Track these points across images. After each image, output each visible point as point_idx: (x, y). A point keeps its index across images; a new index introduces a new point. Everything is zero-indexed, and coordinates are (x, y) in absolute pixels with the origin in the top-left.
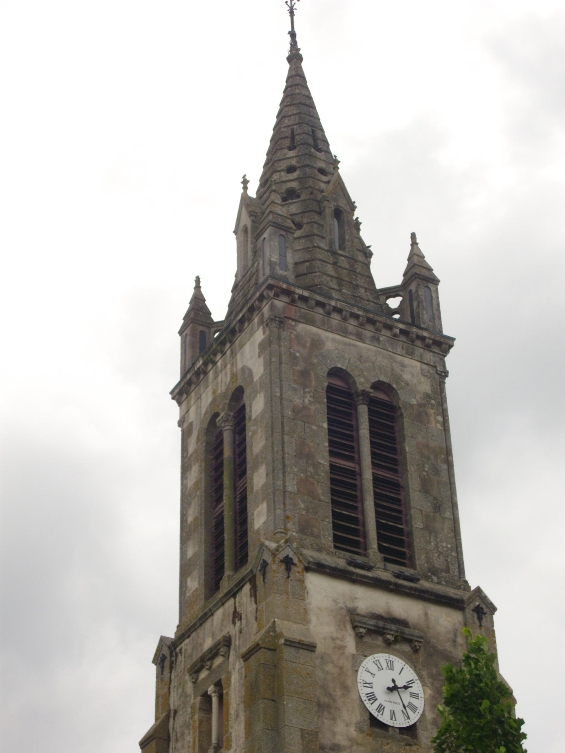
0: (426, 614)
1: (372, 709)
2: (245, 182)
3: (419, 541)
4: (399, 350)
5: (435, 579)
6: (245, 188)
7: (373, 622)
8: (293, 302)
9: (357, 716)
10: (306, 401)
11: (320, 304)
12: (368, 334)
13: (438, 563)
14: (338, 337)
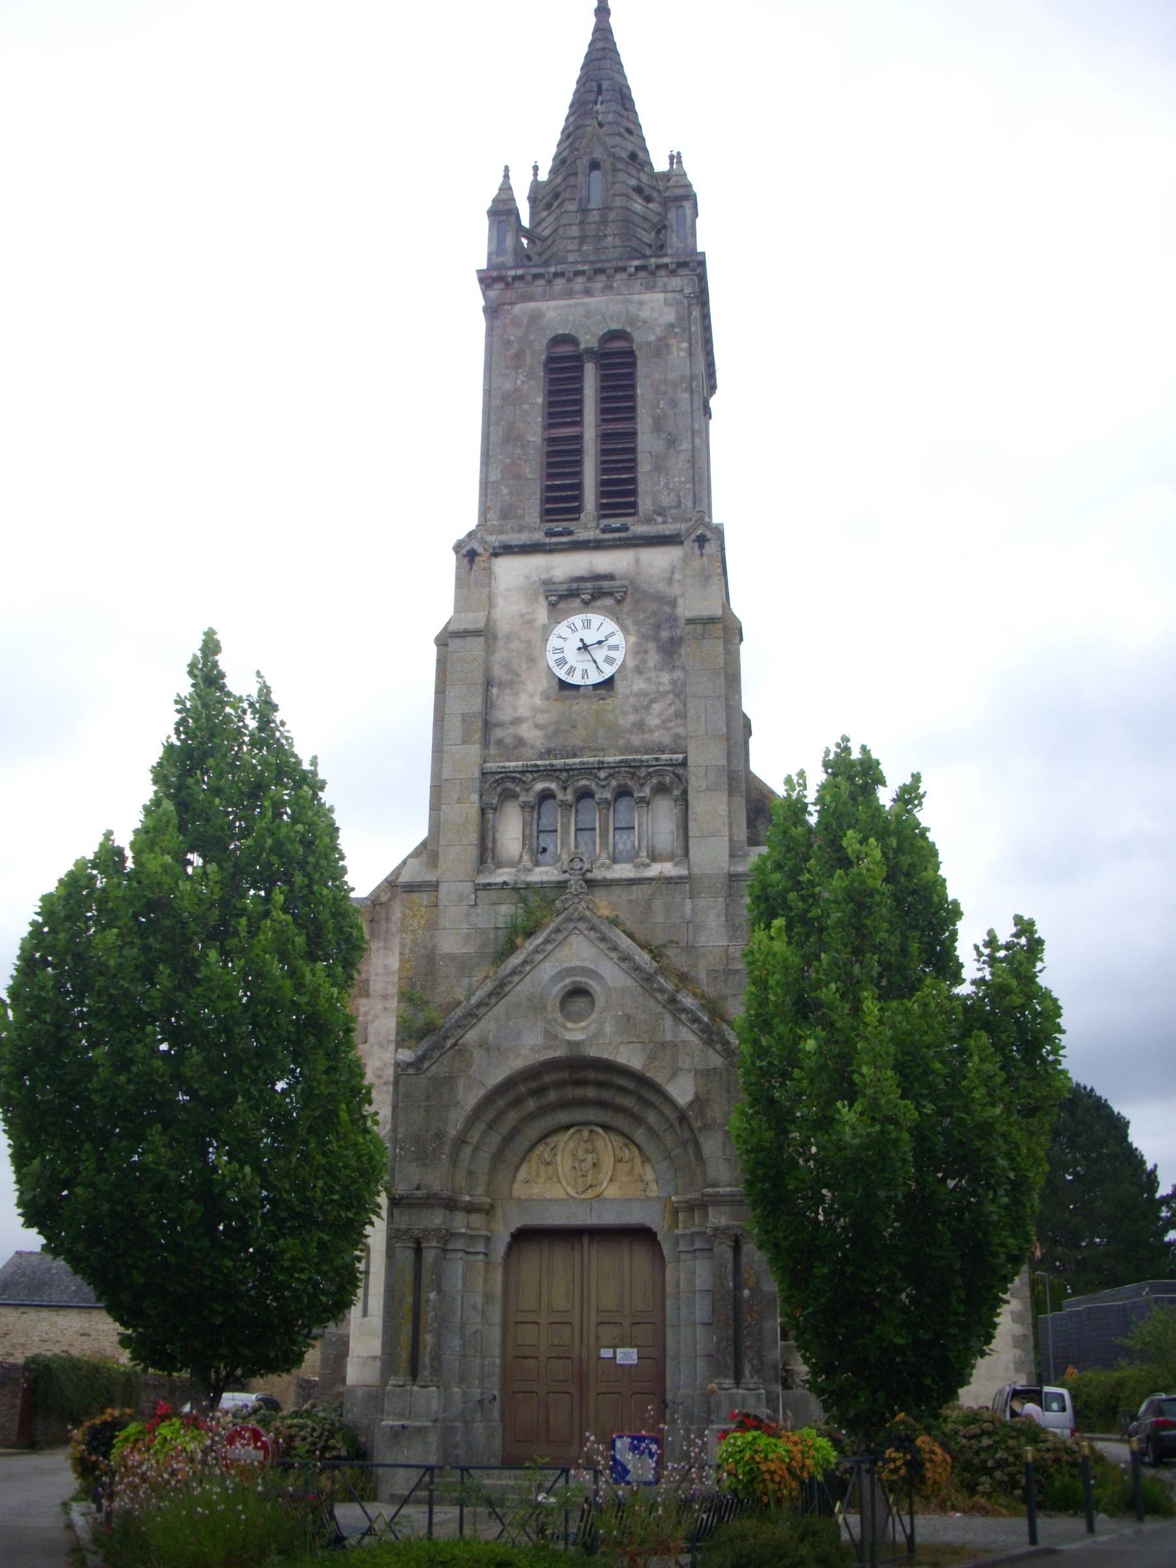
0: (637, 561)
1: (561, 674)
2: (536, 168)
3: (643, 486)
4: (637, 288)
5: (660, 519)
6: (535, 174)
7: (565, 586)
8: (507, 285)
9: (544, 684)
10: (519, 382)
11: (536, 277)
12: (598, 285)
13: (666, 500)
14: (561, 302)
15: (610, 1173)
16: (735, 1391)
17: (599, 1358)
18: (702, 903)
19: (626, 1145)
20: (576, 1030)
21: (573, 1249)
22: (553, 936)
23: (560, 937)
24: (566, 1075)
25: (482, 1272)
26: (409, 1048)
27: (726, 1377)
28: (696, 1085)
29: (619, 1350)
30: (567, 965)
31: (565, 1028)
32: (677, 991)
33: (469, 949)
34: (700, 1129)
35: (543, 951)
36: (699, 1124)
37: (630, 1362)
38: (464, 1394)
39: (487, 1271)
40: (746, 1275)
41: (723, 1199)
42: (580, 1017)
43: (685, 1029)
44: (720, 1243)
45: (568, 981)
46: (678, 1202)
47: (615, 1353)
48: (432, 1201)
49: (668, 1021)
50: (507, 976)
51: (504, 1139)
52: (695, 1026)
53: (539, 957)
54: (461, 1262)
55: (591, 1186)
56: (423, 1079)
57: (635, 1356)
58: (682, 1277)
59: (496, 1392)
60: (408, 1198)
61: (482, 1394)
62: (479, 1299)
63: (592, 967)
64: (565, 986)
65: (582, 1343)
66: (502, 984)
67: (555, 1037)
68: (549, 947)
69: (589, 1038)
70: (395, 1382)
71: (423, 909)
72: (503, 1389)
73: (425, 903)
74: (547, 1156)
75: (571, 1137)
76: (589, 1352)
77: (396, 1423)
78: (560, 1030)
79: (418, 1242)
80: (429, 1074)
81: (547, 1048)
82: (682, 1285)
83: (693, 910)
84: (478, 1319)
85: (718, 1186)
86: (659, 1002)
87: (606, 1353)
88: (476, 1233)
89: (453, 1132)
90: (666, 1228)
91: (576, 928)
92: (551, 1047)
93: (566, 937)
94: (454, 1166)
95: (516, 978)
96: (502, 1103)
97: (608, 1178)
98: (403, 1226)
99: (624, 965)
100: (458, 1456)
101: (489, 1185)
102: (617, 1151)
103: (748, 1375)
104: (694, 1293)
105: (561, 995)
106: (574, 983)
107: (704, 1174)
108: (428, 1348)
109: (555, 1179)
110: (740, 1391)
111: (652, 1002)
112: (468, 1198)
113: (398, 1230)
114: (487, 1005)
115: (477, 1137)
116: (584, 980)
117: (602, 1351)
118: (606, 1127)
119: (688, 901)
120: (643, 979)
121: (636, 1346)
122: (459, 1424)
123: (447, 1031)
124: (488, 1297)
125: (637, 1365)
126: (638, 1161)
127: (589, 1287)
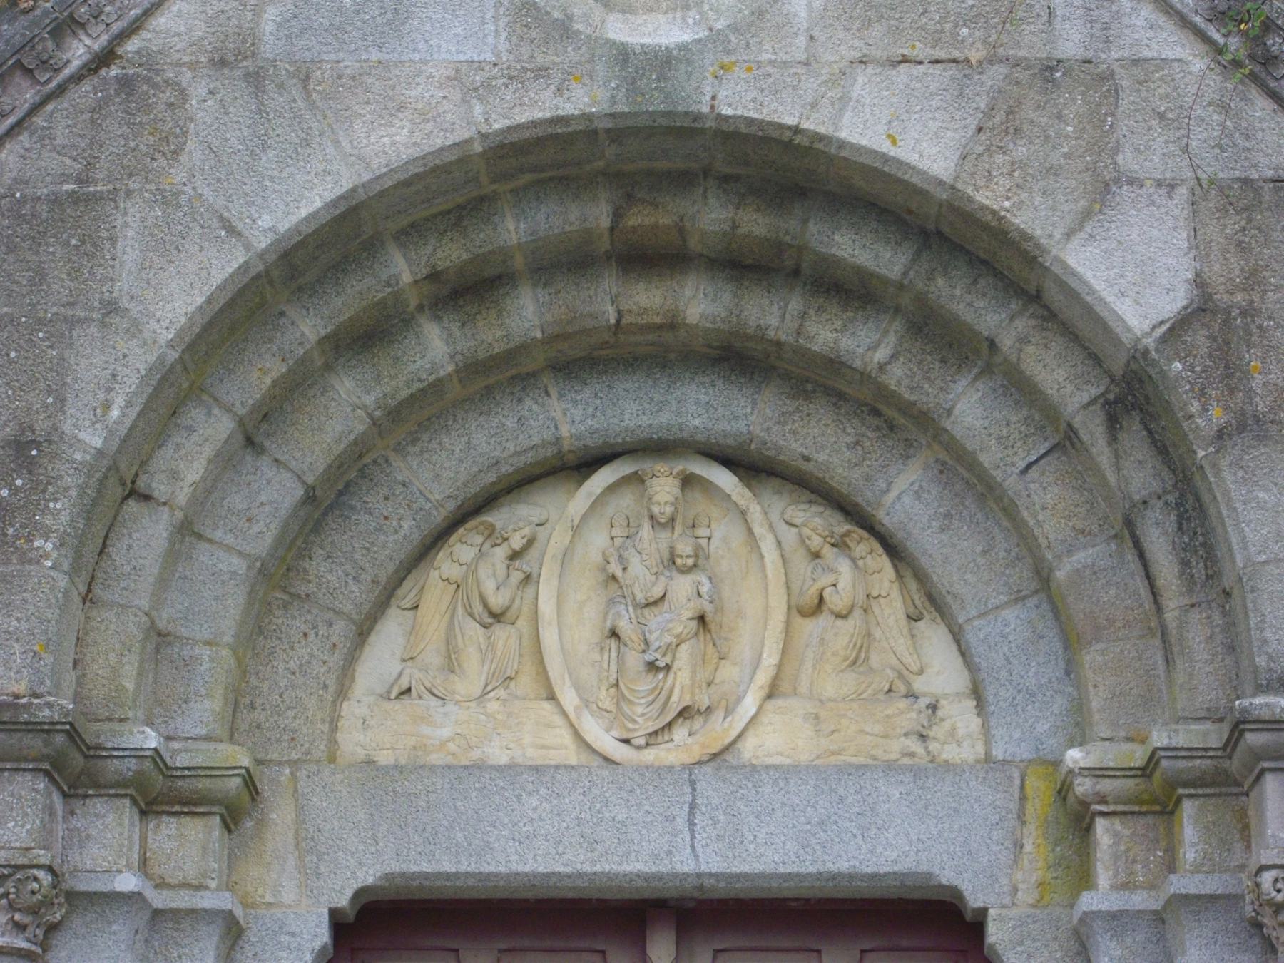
15: (770, 659)
19: (840, 544)
28: (1198, 246)
36: (1217, 413)
46: (1098, 772)
51: (310, 498)
55: (685, 713)
67: (563, 30)
75: (598, 502)
88: (183, 900)
89: (95, 439)
92: (541, 72)
94: (88, 598)
97: (763, 678)
102: (801, 565)
109: (526, 684)
112: (151, 740)
115: (194, 472)
126: (892, 609)
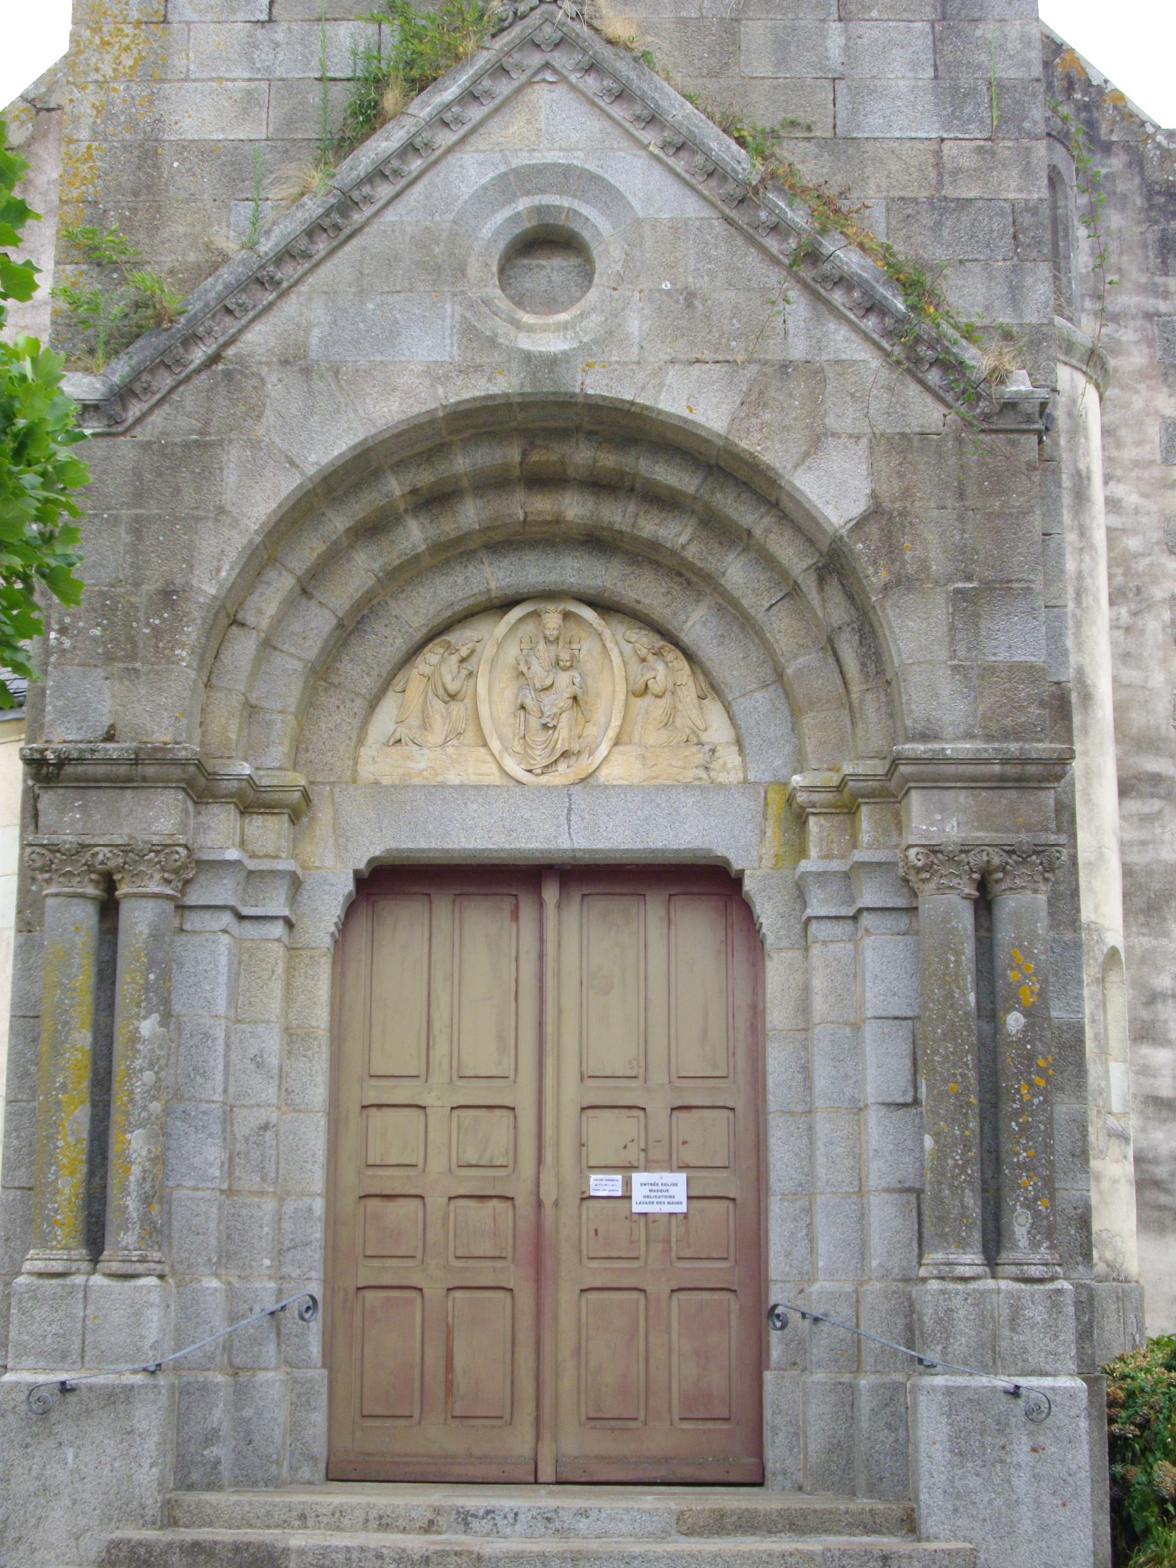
15: (616, 722)
16: (990, 1283)
17: (586, 1198)
18: (869, 32)
19: (658, 654)
20: (545, 329)
21: (515, 916)
22: (486, 83)
23: (504, 88)
24: (512, 454)
25: (280, 969)
26: (87, 370)
27: (963, 1244)
28: (873, 474)
29: (638, 1178)
30: (522, 159)
31: (518, 325)
32: (824, 231)
33: (253, 130)
34: (886, 588)
35: (458, 120)
36: (884, 576)
37: (667, 1209)
38: (231, 1294)
39: (290, 969)
40: (1013, 976)
41: (951, 769)
42: (550, 305)
43: (844, 331)
44: (941, 889)
45: (523, 204)
46: (811, 789)
47: (627, 1183)
48: (150, 771)
49: (799, 308)
50: (359, 184)
51: (341, 625)
52: (870, 323)
53: (446, 138)
54: (225, 939)
55: (565, 754)
56: (125, 449)
57: (681, 1193)
58: (817, 983)
59: (316, 1289)
60: (80, 760)
61: (280, 1293)
62: (272, 1042)
63: (592, 167)
64: (515, 218)
65: (540, 1160)
66: (346, 204)
67: (492, 342)
68: (475, 113)
69: (584, 347)
70: (40, 1266)
71: (129, 30)
72: (329, 1282)
73: (135, 15)
74: (450, 677)
76: (559, 1184)
77: (41, 1378)
78: (503, 329)
79: (109, 883)
80: (143, 434)
81: (468, 370)
82: (819, 1005)
83: (847, 49)
84: (270, 1093)
85: (936, 737)
86: (775, 261)
87: (604, 1184)
88: (266, 865)
90: (767, 863)
91: (547, 66)
92: (478, 368)
93: (519, 90)
94: (208, 685)
95: (384, 191)
96: (339, 522)
97: (611, 733)
98: (68, 839)
99: (679, 165)
100: (218, 1462)
101: (299, 746)
102: (634, 665)
103: (1023, 1243)
104: (856, 1027)
105: (502, 245)
106: (539, 210)
107: (892, 711)
108: (136, 1170)
109: (470, 736)
110: (1003, 1284)
111: (752, 258)
112: (246, 769)
113: (53, 848)
114: (306, 255)
115: (271, 609)
116: (565, 202)
117: (594, 1178)
118: (605, 606)
119: (835, 27)
120: (728, 199)
121: (681, 1168)
122: (220, 1378)
123: (193, 321)
124: (293, 1037)
125: (686, 1216)
126: (689, 692)
127: (560, 1012)
